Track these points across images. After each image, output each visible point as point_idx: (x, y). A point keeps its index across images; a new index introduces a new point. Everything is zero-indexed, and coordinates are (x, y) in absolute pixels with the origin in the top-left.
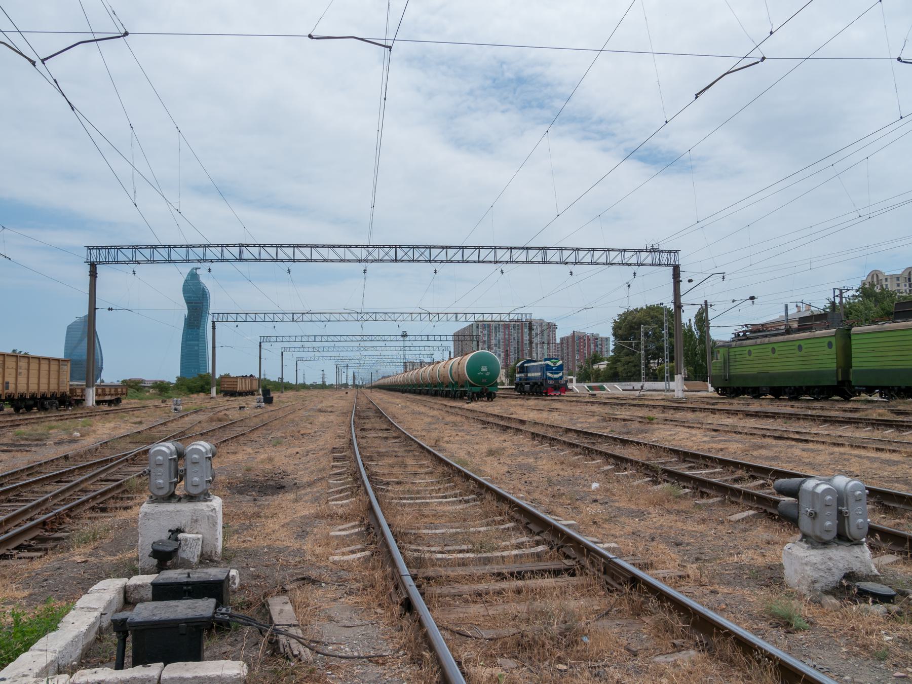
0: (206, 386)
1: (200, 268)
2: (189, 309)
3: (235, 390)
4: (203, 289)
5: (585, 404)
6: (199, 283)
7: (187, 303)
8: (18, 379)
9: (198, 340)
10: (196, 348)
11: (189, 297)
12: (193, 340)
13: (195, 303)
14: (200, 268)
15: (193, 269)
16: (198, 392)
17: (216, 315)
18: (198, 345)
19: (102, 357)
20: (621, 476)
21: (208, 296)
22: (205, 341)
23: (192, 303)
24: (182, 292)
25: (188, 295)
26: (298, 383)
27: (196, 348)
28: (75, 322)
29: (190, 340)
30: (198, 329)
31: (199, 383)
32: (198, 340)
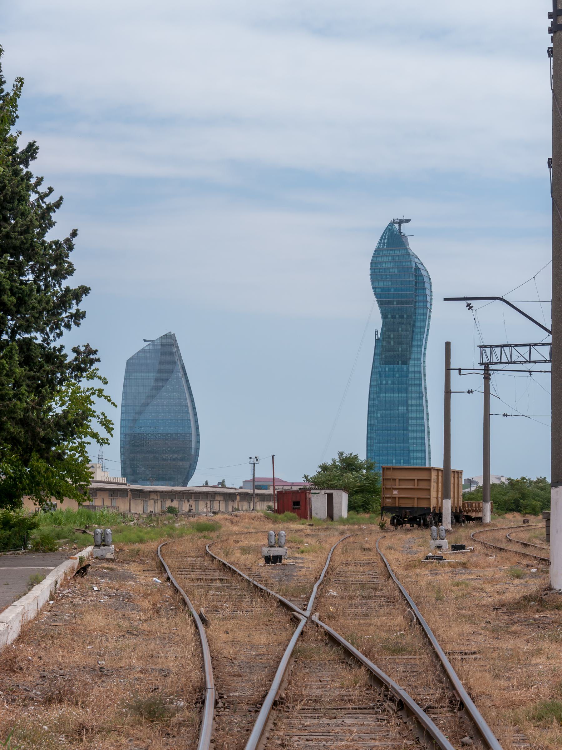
0: (522, 501)
1: (408, 221)
2: (384, 316)
3: (424, 505)
4: (417, 269)
5: (460, 479)
6: (408, 255)
7: (381, 303)
8: (228, 487)
9: (406, 391)
10: (402, 408)
11: (383, 289)
12: (393, 391)
13: (399, 303)
14: (408, 221)
15: (392, 223)
16: (511, 510)
17: (497, 350)
18: (405, 402)
19: (197, 428)
20: (422, 336)
21: (427, 286)
22: (421, 392)
23: (390, 303)
24: (369, 279)
25: (382, 284)
26: (493, 480)
27: (402, 408)
28: (142, 351)
29: (387, 391)
30: (405, 363)
31: (513, 495)
32: (406, 391)
